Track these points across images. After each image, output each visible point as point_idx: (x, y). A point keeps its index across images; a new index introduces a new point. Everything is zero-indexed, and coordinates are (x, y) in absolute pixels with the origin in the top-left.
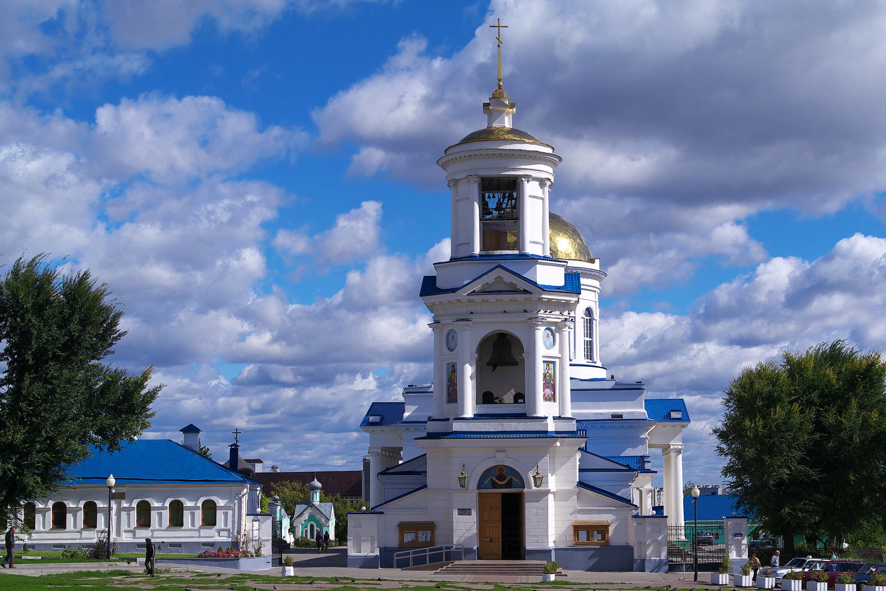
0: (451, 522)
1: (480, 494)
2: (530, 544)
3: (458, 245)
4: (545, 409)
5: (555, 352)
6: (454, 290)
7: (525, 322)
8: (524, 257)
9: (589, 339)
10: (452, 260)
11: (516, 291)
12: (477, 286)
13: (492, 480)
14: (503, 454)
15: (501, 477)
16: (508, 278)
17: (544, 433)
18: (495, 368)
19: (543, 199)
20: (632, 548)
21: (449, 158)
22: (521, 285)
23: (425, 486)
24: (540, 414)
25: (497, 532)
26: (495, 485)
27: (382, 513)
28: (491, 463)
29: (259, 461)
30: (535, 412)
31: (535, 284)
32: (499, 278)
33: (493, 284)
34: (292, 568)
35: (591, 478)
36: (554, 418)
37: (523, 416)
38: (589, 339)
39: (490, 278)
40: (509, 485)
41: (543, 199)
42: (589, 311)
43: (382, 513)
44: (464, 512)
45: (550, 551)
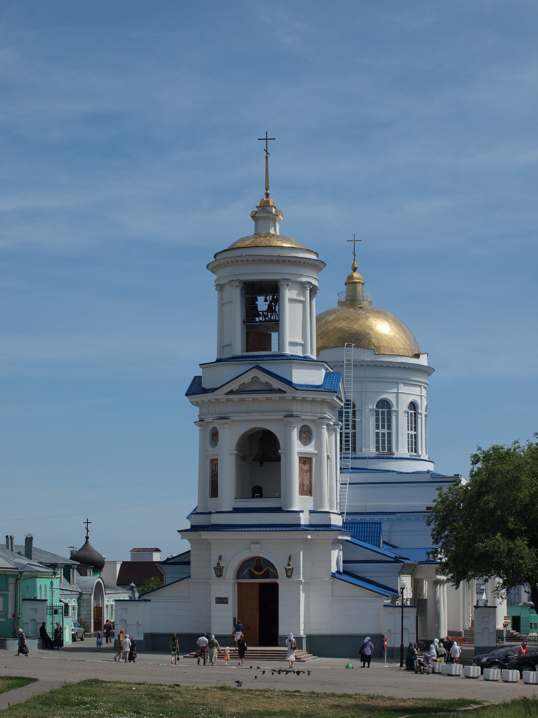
0: (210, 610)
1: (239, 584)
2: (282, 631)
3: (223, 347)
4: (301, 504)
5: (310, 449)
6: (213, 390)
7: (282, 420)
8: (282, 357)
9: (413, 433)
10: (218, 361)
11: (272, 391)
12: (234, 386)
13: (250, 570)
14: (258, 546)
15: (259, 568)
16: (264, 378)
17: (296, 527)
18: (262, 463)
19: (303, 302)
20: (383, 636)
21: (218, 263)
22: (276, 384)
23: (190, 576)
24: (296, 508)
25: (255, 621)
26: (253, 576)
27: (149, 601)
28: (247, 555)
29: (157, 550)
30: (291, 506)
31: (289, 383)
32: (255, 379)
33: (250, 384)
34: (459, 666)
35: (353, 567)
36: (311, 512)
37: (279, 510)
38: (413, 433)
39: (247, 379)
40: (266, 575)
41: (303, 302)
42: (413, 406)
43: (149, 601)
44: (222, 601)
45: (302, 638)
